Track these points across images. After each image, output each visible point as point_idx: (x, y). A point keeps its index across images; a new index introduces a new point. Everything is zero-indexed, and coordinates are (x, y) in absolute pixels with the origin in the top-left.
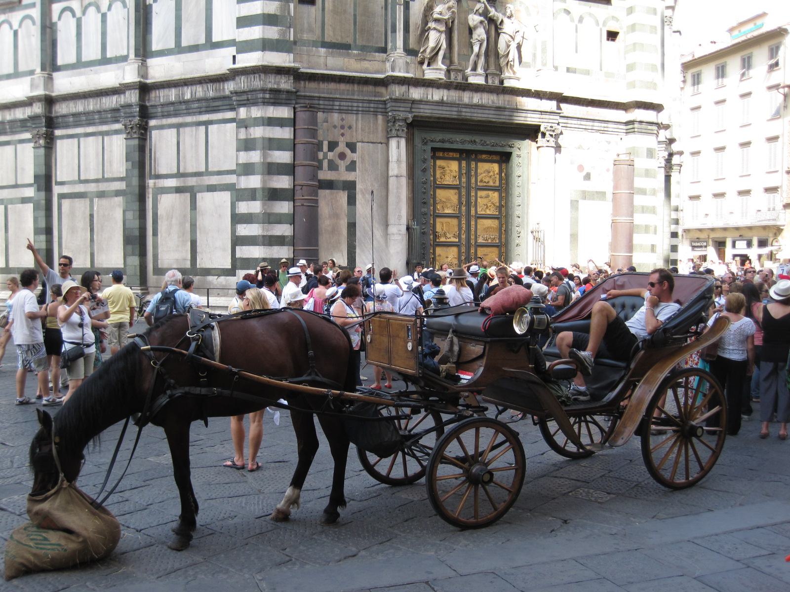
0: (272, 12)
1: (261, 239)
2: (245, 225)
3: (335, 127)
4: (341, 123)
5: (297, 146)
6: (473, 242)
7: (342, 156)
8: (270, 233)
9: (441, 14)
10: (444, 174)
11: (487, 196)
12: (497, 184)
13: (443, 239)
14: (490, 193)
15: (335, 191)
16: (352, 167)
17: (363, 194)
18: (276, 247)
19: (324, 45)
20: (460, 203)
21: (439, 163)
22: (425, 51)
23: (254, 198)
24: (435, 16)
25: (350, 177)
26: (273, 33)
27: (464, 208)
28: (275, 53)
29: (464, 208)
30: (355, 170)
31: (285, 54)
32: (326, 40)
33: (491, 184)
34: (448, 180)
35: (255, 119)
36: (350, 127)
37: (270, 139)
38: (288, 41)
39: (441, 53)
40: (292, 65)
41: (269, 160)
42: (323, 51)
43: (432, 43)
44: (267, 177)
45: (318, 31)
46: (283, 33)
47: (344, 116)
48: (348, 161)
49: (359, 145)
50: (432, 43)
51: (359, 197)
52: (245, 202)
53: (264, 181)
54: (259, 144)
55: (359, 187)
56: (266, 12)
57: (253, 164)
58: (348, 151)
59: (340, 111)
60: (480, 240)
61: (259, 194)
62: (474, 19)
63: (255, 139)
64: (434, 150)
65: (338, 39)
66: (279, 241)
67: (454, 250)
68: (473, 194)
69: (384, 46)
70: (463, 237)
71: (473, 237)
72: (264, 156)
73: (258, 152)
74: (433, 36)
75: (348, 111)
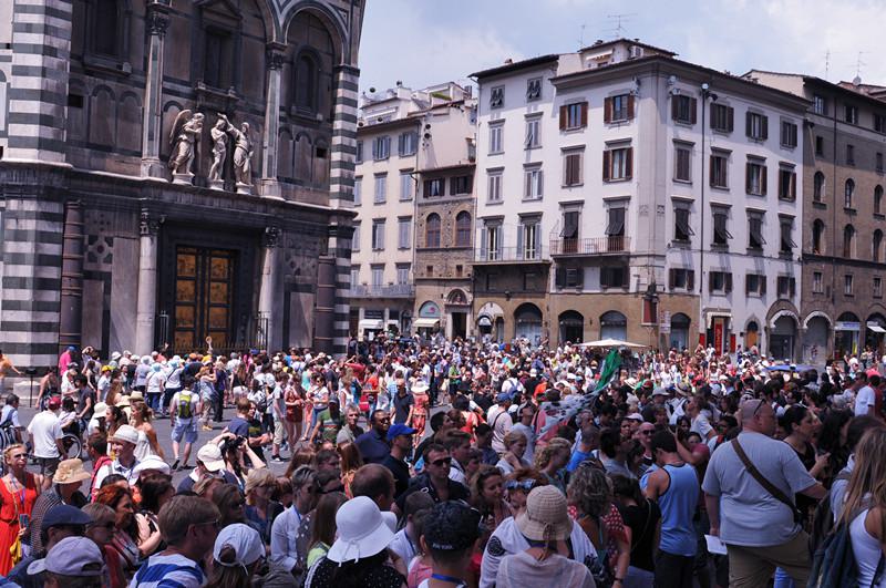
0: (48, 114)
1: (30, 326)
2: (12, 312)
3: (95, 222)
4: (100, 219)
5: (67, 241)
6: (207, 277)
7: (101, 249)
8: (38, 320)
9: (192, 127)
10: (183, 266)
11: (218, 287)
12: (226, 277)
13: (181, 325)
14: (220, 284)
15: (93, 281)
16: (109, 260)
17: (117, 284)
18: (43, 333)
19: (89, 146)
20: (196, 292)
21: (180, 257)
22: (175, 159)
23: (23, 287)
24: (187, 129)
25: (105, 268)
26: (49, 133)
27: (199, 298)
28: (49, 152)
29: (200, 273)
30: (111, 262)
31: (58, 154)
32: (91, 141)
33: (221, 277)
34: (187, 272)
35: (27, 212)
36: (108, 223)
37: (42, 232)
38: (61, 142)
39: (190, 163)
40: (37, 161)
41: (40, 252)
42: (87, 151)
43: (182, 153)
44: (38, 268)
45: (84, 134)
46: (57, 134)
47: (104, 213)
48: (105, 254)
49: (115, 239)
50: (182, 153)
51: (114, 287)
52: (12, 290)
53: (35, 272)
54: (32, 237)
55: (114, 278)
56: (43, 113)
57: (24, 254)
58: (105, 245)
59: (101, 208)
60: (211, 326)
61: (29, 283)
62: (216, 133)
63: (26, 231)
64: (178, 245)
65: (100, 142)
66: (47, 327)
67: (190, 334)
68: (207, 285)
69: (11, 101)
70: (198, 323)
71: (205, 323)
72: (37, 248)
73: (30, 244)
74: (183, 147)
75: (107, 208)
